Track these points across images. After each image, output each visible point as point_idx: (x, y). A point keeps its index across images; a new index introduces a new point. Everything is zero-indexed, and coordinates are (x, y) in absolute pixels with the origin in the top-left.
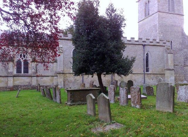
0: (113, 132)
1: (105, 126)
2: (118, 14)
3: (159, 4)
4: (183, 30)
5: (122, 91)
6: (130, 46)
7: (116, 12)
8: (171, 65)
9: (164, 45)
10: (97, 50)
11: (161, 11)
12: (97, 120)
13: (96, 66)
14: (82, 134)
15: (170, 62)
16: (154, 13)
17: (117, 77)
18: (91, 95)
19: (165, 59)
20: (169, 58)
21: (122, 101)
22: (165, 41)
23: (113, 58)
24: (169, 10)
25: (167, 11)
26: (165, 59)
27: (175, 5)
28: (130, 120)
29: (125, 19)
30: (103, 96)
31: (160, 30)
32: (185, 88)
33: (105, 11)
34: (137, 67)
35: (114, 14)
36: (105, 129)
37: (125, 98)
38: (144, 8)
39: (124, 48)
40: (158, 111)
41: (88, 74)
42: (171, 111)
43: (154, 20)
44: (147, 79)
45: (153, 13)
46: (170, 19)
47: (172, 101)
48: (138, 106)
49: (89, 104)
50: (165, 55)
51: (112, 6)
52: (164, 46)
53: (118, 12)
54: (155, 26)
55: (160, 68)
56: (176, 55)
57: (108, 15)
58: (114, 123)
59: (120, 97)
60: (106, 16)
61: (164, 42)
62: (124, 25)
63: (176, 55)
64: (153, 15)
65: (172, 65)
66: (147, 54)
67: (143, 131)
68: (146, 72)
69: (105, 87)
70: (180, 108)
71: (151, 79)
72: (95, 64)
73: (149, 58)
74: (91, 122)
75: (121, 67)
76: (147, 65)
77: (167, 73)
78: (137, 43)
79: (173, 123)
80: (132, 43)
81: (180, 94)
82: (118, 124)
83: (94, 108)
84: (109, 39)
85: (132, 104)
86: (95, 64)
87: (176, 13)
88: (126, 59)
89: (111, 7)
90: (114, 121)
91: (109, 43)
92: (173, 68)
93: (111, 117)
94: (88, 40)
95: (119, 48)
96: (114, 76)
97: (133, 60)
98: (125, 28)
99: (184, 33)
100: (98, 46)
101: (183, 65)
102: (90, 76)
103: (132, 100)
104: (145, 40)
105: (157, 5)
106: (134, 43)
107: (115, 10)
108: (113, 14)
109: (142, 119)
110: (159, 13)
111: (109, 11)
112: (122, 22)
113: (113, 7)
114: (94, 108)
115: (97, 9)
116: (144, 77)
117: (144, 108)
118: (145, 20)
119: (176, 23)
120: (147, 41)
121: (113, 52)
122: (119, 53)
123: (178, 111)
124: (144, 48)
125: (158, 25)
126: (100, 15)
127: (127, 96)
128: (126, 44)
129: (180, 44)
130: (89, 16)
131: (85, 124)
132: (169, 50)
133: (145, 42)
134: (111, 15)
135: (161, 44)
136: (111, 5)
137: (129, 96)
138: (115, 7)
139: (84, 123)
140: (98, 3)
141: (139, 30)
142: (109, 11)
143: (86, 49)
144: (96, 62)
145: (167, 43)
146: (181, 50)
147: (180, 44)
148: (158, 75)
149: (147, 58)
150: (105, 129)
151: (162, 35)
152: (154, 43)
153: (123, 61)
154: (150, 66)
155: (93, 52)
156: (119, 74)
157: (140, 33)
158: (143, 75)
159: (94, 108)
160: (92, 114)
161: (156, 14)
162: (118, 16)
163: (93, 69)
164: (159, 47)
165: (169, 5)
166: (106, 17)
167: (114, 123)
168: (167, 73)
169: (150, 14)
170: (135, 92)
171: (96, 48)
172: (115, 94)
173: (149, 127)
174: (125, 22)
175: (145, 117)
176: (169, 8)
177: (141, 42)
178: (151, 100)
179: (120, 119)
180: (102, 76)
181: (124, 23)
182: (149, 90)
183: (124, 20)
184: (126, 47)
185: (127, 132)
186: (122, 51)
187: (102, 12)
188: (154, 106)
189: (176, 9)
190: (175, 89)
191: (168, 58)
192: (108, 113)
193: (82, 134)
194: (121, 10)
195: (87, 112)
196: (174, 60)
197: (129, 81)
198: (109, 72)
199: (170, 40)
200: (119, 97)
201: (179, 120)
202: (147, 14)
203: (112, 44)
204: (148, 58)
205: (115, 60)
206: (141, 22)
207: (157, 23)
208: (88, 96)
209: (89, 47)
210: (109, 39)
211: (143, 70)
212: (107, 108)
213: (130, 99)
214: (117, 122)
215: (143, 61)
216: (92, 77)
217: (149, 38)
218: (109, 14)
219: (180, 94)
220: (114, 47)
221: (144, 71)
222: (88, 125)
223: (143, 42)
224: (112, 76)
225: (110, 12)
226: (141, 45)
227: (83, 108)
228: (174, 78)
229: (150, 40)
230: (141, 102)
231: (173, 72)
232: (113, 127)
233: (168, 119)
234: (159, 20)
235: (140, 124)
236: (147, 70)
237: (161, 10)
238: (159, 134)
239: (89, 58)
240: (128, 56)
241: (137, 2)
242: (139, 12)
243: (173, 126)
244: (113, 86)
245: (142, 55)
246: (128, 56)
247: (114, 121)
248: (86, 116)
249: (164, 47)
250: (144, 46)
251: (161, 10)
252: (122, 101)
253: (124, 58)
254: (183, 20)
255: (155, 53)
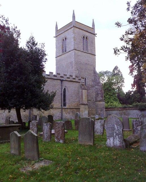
0: (44, 169)
1: (33, 164)
2: (39, 48)
3: (75, 42)
4: (95, 69)
5: (46, 127)
6: (49, 81)
7: (37, 46)
8: (85, 101)
9: (79, 81)
10: (17, 84)
11: (76, 49)
12: (24, 159)
13: (15, 101)
14: (11, 176)
15: (84, 97)
16: (71, 50)
17: (35, 112)
18: (16, 132)
19: (80, 94)
20: (83, 94)
21: (46, 137)
22: (80, 78)
23: (35, 92)
24: (84, 49)
25: (82, 50)
26: (80, 94)
27: (89, 45)
28: (58, 156)
29: (46, 54)
30: (31, 133)
31: (76, 67)
32: (100, 122)
33: (26, 43)
34: (57, 103)
35: (35, 47)
36: (34, 167)
37: (49, 134)
38: (61, 44)
39: (45, 83)
40: (81, 145)
41: (5, 109)
42: (92, 144)
43: (71, 57)
44: (64, 113)
45: (70, 50)
46: (84, 57)
47: (93, 134)
48: (61, 141)
49: (13, 143)
50: (80, 90)
51: (33, 39)
52: (80, 82)
53: (39, 46)
54: (71, 63)
55: (76, 102)
56: (89, 91)
57: (29, 48)
58: (42, 160)
59: (43, 133)
60: (26, 48)
61: (79, 78)
62: (45, 60)
63: (89, 91)
64: (70, 52)
65: (86, 100)
66: (65, 89)
67: (72, 165)
68: (64, 106)
69: (24, 122)
70: (98, 141)
71: (68, 114)
72: (15, 98)
73: (66, 93)
74: (17, 162)
75: (42, 101)
76: (65, 100)
77: (82, 107)
78: (56, 78)
79: (96, 155)
80: (52, 77)
81: (97, 128)
82: (46, 160)
83: (19, 146)
84: (30, 73)
85: (56, 139)
86: (15, 98)
87: (89, 53)
88: (47, 93)
89: (31, 40)
90: (42, 158)
91: (31, 76)
92: (87, 102)
93: (38, 154)
94: (7, 72)
95: (40, 82)
96: (32, 110)
97: (54, 96)
98: (46, 62)
99: (96, 71)
100: (18, 79)
101: (95, 100)
102: (7, 111)
103: (56, 135)
104: (63, 76)
105: (73, 43)
106: (52, 78)
107: (36, 44)
108: (34, 48)
109: (68, 153)
110: (76, 51)
111: (30, 44)
112: (43, 56)
113: (35, 40)
114: (19, 146)
115: (17, 41)
116: (62, 111)
117: (67, 143)
118: (62, 56)
119: (89, 62)
120: (64, 76)
121: (34, 86)
122: (40, 87)
123: (97, 144)
124: (62, 83)
125: (74, 62)
126: (20, 47)
127: (51, 132)
128: (46, 78)
129: (93, 81)
130: (9, 47)
131: (10, 164)
132: (83, 86)
133: (63, 77)
134: (32, 48)
135: (77, 80)
136: (31, 38)
137: (53, 131)
138: (36, 41)
139: (8, 163)
140: (19, 35)
141: (56, 65)
142: (30, 44)
143: (4, 82)
144: (15, 96)
145: (82, 79)
146: (93, 86)
147: (93, 81)
148: (74, 110)
149: (65, 92)
150: (34, 167)
151: (77, 72)
152: (71, 79)
153: (44, 95)
154: (67, 101)
155: (12, 84)
156: (39, 109)
157: (57, 68)
158: (60, 110)
159: (19, 146)
160: (17, 153)
161: (72, 51)
162: (39, 50)
163: (12, 104)
164: (75, 83)
165: (84, 45)
166: (27, 50)
167: (42, 160)
168: (82, 107)
169: (67, 50)
170: (59, 127)
171: (16, 80)
172: (37, 130)
173: (76, 161)
174: (46, 57)
175: (71, 151)
176: (84, 47)
177: (59, 77)
178: (72, 134)
179: (48, 155)
180: (22, 111)
181: (45, 58)
182: (68, 124)
183: (45, 55)
184: (46, 81)
185: (57, 168)
186: (43, 85)
187: (22, 44)
188: (76, 140)
189: (89, 48)
190: (37, 117)
191: (82, 93)
192: (35, 150)
193: (11, 176)
194: (42, 45)
195: (10, 152)
196: (87, 95)
197: (48, 116)
198: (29, 106)
199: (84, 77)
200: (42, 133)
201: (100, 152)
202: (64, 51)
203: (33, 78)
204: (65, 93)
205: (35, 94)
206: (58, 58)
207: (73, 60)
208: (12, 134)
209: (8, 79)
210: (30, 73)
211: (61, 104)
212: (35, 145)
213: (54, 134)
214: (45, 159)
215: (60, 96)
216: (10, 112)
217: (66, 74)
218: (30, 47)
219: (97, 128)
220: (35, 81)
221: (62, 105)
222: (13, 165)
223: (61, 77)
224: (30, 110)
225: (31, 45)
226: (59, 80)
227: (3, 147)
228: (87, 112)
229: (61, 75)
230: (64, 137)
231: (87, 107)
232: (42, 164)
233: (91, 151)
234: (75, 58)
235: (67, 159)
236: (65, 105)
237: (77, 48)
238: (86, 166)
239: (8, 91)
240: (48, 91)
241: (54, 37)
242: (57, 47)
243: (96, 158)
244: (35, 122)
245: (60, 90)
246: (48, 91)
247: (42, 158)
248: (11, 156)
249: (79, 83)
250: (62, 81)
251: (77, 48)
252: (46, 137)
253: (44, 92)
254: (95, 59)
255: (71, 88)
